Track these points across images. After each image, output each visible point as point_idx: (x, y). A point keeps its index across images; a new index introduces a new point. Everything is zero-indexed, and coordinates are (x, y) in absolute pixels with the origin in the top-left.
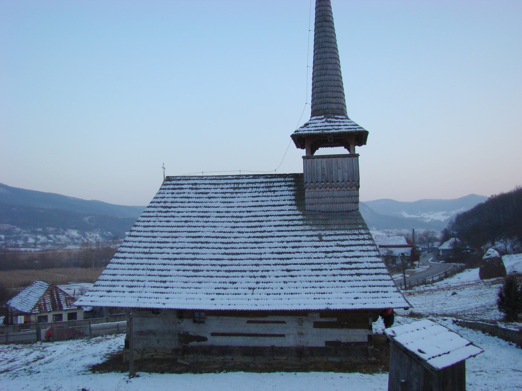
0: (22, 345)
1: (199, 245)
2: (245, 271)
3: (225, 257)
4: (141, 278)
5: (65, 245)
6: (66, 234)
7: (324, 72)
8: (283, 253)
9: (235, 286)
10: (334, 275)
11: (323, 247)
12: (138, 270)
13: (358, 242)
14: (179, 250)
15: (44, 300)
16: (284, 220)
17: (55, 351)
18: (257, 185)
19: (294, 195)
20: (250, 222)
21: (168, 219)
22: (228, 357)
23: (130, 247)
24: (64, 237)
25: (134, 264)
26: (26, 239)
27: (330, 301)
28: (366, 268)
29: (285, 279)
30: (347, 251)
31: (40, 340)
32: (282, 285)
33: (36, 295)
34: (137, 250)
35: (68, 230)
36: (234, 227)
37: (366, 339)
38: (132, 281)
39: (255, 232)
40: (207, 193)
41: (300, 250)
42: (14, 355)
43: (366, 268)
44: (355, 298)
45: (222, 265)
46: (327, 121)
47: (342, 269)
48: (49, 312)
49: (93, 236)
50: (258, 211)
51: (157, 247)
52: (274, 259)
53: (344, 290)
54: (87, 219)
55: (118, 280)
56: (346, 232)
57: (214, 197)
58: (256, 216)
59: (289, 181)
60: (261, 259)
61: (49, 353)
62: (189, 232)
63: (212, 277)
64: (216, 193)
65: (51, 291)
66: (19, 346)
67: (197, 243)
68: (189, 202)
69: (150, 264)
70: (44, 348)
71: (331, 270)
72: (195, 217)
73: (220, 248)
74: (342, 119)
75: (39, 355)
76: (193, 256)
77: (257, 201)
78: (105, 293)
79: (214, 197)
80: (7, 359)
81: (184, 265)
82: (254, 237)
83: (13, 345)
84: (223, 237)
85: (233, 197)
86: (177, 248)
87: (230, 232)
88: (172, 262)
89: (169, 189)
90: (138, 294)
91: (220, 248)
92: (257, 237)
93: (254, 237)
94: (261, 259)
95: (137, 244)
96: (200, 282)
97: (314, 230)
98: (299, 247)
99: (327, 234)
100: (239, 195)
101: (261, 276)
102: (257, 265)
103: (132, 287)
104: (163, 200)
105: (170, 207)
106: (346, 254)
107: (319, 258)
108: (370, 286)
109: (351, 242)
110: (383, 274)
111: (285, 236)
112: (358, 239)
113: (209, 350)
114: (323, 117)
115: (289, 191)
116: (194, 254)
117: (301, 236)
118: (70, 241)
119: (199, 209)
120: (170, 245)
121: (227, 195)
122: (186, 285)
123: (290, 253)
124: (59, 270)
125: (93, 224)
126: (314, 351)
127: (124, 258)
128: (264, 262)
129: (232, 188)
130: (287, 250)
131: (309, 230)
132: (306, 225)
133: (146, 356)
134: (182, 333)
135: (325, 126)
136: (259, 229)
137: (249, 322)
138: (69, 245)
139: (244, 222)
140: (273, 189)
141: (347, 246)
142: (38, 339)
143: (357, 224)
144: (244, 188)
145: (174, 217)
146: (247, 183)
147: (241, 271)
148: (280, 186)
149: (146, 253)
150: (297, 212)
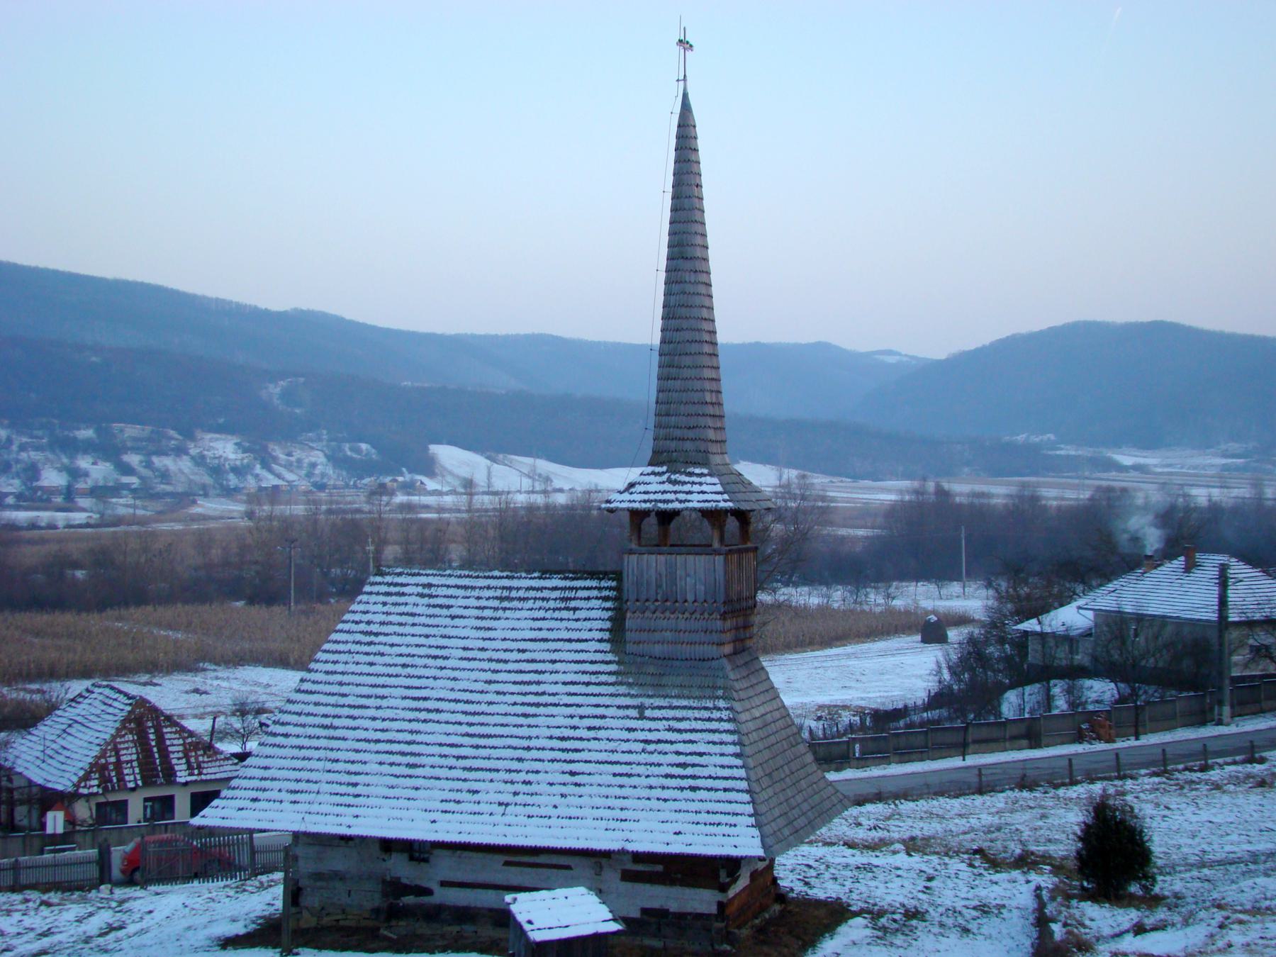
1: (423, 715)
2: (498, 770)
3: (466, 740)
4: (314, 776)
5: (187, 498)
6: (193, 452)
7: (673, 371)
8: (569, 738)
9: (476, 797)
10: (651, 787)
12: (310, 759)
14: (386, 724)
15: (117, 751)
16: (584, 672)
17: (150, 912)
18: (546, 594)
19: (610, 619)
20: (521, 672)
21: (371, 658)
22: (468, 928)
23: (297, 714)
24: (185, 464)
26: (33, 472)
27: (632, 836)
28: (710, 777)
29: (564, 790)
30: (684, 742)
31: (110, 881)
33: (89, 735)
34: (310, 720)
35: (199, 434)
36: (489, 682)
37: (713, 909)
39: (525, 694)
40: (449, 607)
41: (601, 734)
42: (48, 921)
43: (710, 777)
45: (458, 758)
46: (670, 481)
47: (667, 776)
48: (133, 789)
49: (299, 461)
51: (348, 717)
52: (552, 749)
53: (662, 816)
55: (273, 779)
57: (462, 617)
58: (533, 661)
59: (606, 588)
60: (529, 749)
61: (136, 916)
62: (408, 687)
63: (439, 779)
65: (139, 721)
66: (54, 897)
68: (414, 625)
69: (332, 749)
70: (121, 902)
71: (647, 776)
73: (460, 723)
74: (702, 475)
75: (111, 921)
76: (409, 737)
77: (540, 629)
78: (248, 804)
79: (462, 617)
80: (32, 929)
82: (523, 704)
83: (34, 895)
84: (467, 702)
85: (495, 619)
86: (384, 720)
87: (482, 692)
88: (373, 747)
89: (378, 594)
90: (306, 807)
91: (460, 723)
92: (529, 704)
93: (523, 704)
94: (529, 749)
95: (311, 709)
96: (417, 789)
98: (600, 728)
101: (524, 782)
102: (520, 760)
103: (296, 792)
104: (366, 618)
105: (377, 634)
106: (681, 747)
107: (630, 752)
108: (708, 812)
109: (695, 725)
110: (738, 791)
111: (578, 706)
112: (709, 720)
113: (435, 914)
114: (664, 469)
115: (604, 609)
116: (411, 732)
118: (208, 480)
119: (432, 641)
120: (371, 712)
121: (487, 613)
123: (581, 739)
124: (166, 613)
125: (297, 411)
127: (286, 735)
128: (534, 754)
129: (497, 598)
130: (577, 733)
131: (625, 695)
132: (621, 684)
133: (326, 921)
134: (388, 878)
135: (664, 492)
136: (534, 688)
137: (507, 864)
138: (206, 495)
139: (509, 672)
140: (573, 604)
141: (686, 731)
142: (104, 876)
143: (715, 688)
144: (520, 599)
145: (382, 654)
146: (528, 589)
147: (490, 770)
148: (588, 599)
149: (326, 727)
150: (610, 657)
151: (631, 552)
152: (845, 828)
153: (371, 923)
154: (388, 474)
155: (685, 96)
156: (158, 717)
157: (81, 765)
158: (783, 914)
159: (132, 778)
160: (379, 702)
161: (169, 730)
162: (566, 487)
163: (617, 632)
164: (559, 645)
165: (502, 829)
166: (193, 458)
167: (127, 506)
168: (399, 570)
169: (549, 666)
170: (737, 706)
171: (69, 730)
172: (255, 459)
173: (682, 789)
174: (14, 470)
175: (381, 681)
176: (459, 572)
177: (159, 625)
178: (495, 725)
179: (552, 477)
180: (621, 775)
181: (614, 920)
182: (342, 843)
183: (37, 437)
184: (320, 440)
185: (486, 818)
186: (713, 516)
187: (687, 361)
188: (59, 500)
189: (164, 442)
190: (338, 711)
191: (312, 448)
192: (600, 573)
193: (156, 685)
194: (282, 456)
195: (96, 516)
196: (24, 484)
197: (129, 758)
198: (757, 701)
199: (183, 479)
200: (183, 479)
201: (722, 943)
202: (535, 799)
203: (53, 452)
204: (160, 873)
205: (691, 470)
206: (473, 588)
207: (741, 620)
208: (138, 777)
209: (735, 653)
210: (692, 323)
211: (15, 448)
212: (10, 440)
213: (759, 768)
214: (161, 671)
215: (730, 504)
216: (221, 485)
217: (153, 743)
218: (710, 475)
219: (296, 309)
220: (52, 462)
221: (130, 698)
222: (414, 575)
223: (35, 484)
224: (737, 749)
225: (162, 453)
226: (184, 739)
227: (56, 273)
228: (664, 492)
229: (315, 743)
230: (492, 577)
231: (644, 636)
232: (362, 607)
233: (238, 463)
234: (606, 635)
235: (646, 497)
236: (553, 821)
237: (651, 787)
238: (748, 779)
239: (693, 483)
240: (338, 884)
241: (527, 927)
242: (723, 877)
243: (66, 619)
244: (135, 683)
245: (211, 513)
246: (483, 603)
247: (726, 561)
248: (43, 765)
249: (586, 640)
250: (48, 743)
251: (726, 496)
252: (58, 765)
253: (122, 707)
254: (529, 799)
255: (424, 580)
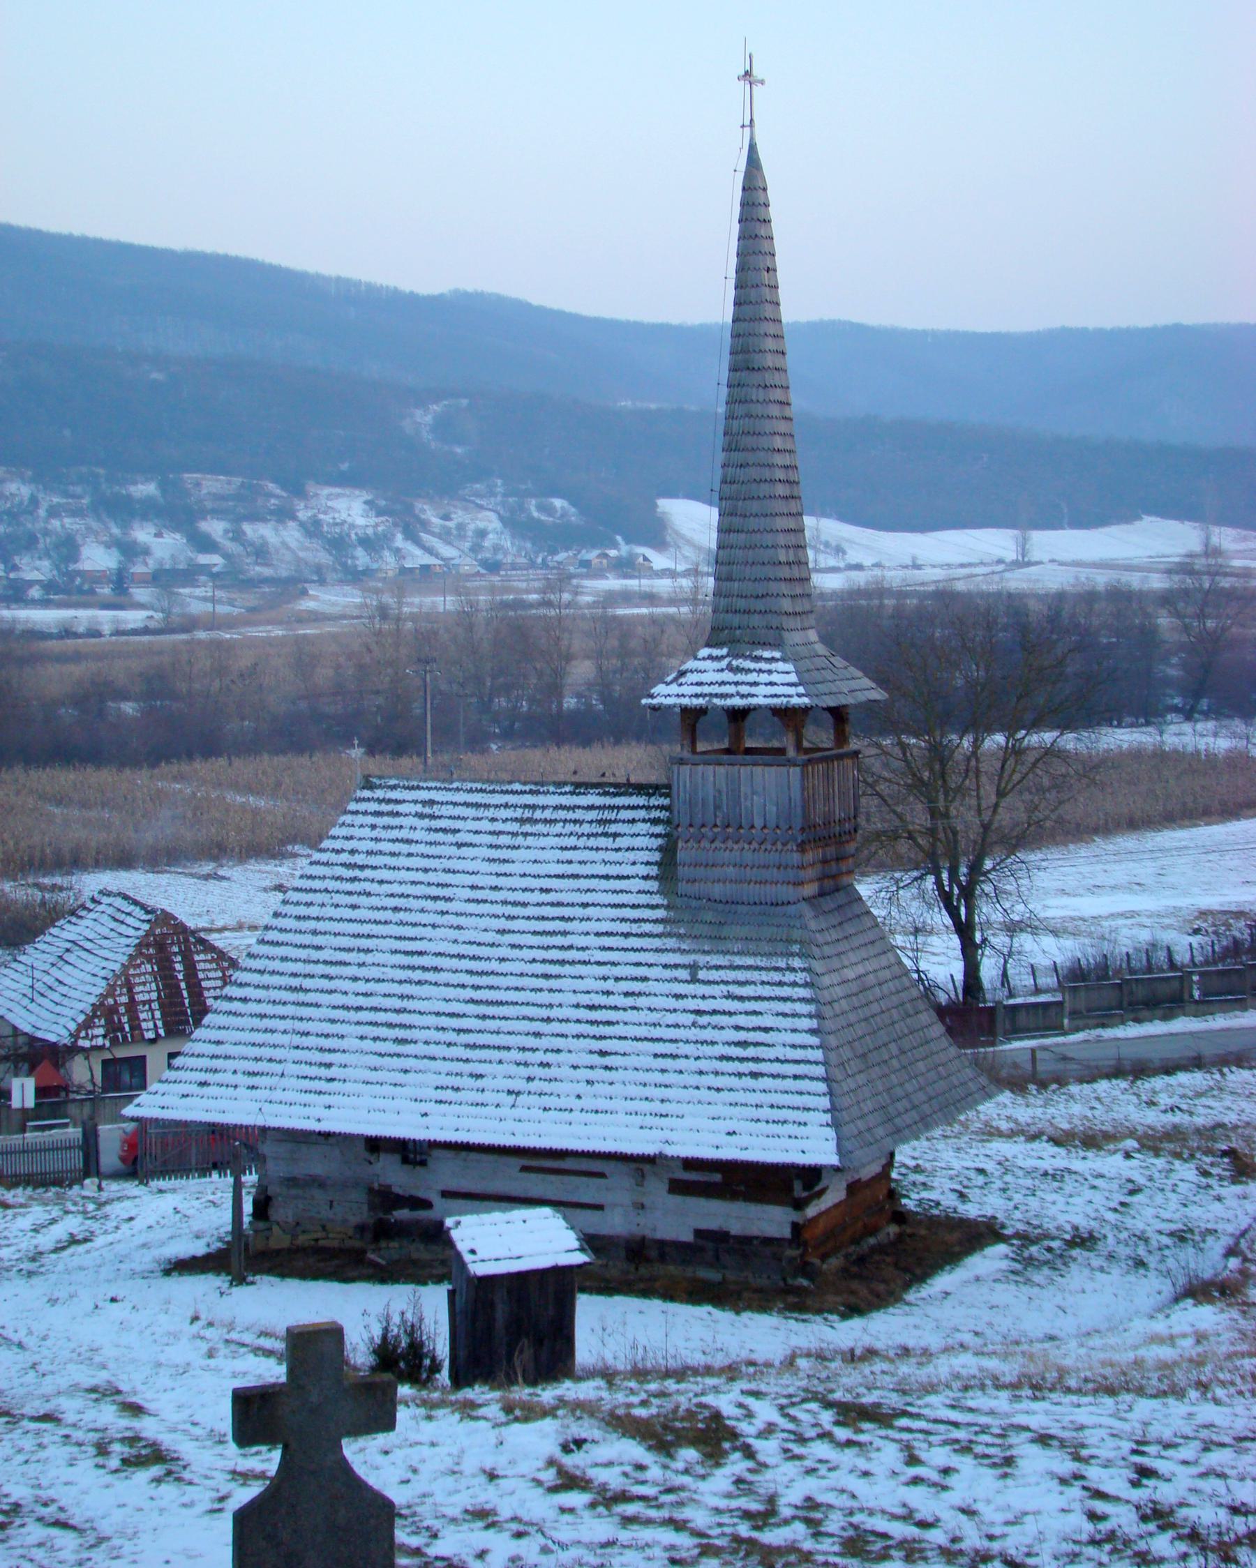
0: (29, 1190)
1: (418, 975)
2: (509, 1048)
4: (278, 1053)
5: (293, 586)
8: (600, 1007)
9: (480, 1083)
10: (701, 1073)
11: (694, 997)
12: (272, 1031)
13: (779, 991)
14: (371, 987)
16: (623, 920)
17: (131, 1219)
18: (579, 814)
19: (660, 849)
20: (543, 918)
24: (291, 534)
25: (265, 1016)
26: (68, 548)
29: (591, 1074)
30: (747, 1013)
31: (98, 1174)
32: (582, 1088)
34: (276, 980)
35: (311, 488)
36: (502, 932)
37: (786, 1232)
38: (257, 1059)
41: (642, 1002)
43: (777, 1060)
44: (729, 1134)
45: (459, 1031)
46: (730, 668)
47: (722, 1058)
48: (153, 1041)
49: (461, 527)
50: (567, 891)
52: (578, 1021)
53: (713, 1110)
54: (424, 418)
55: (227, 1057)
56: (758, 961)
58: (559, 904)
59: (656, 807)
60: (548, 1020)
62: (400, 938)
63: (434, 1058)
64: (476, 832)
65: (161, 946)
67: (413, 968)
68: (410, 855)
71: (698, 1058)
72: (417, 897)
73: (463, 986)
74: (773, 660)
75: (75, 1231)
76: (398, 1003)
77: (570, 862)
78: (194, 1089)
81: (376, 1024)
82: (544, 961)
84: (474, 958)
86: (368, 981)
87: (493, 945)
89: (365, 813)
91: (463, 986)
92: (552, 962)
93: (544, 961)
94: (548, 1020)
96: (406, 1071)
97: (683, 952)
98: (640, 994)
99: (713, 963)
100: (530, 841)
101: (541, 1064)
102: (537, 1035)
103: (254, 1074)
105: (362, 867)
106: (742, 1020)
107: (677, 1026)
108: (772, 1106)
110: (812, 1079)
111: (614, 964)
112: (781, 984)
114: (724, 651)
115: (652, 835)
116: (402, 997)
117: (650, 965)
118: (324, 558)
119: (432, 877)
121: (504, 840)
122: (373, 1076)
123: (615, 1008)
124: (245, 768)
125: (459, 450)
126: (666, 1250)
127: (245, 1000)
128: (556, 1027)
131: (673, 951)
132: (669, 935)
133: (302, 1239)
134: (376, 1186)
135: (723, 683)
136: (559, 940)
137: (525, 1169)
138: (322, 582)
139: (528, 918)
140: (613, 828)
141: (749, 998)
142: (91, 1167)
143: (789, 941)
144: (546, 821)
145: (369, 894)
146: (556, 808)
148: (633, 821)
150: (657, 899)
151: (682, 762)
152: (1131, 1108)
153: (357, 1244)
154: (594, 547)
155: (752, 148)
156: (186, 940)
157: (81, 1006)
158: (900, 1237)
159: (151, 1025)
160: (362, 957)
161: (202, 957)
162: (867, 562)
163: (667, 866)
164: (593, 883)
165: (510, 1125)
166: (302, 525)
167: (205, 599)
168: (392, 782)
169: (579, 912)
170: (818, 966)
171: (67, 956)
172: (395, 525)
173: (740, 1075)
174: (41, 546)
175: (365, 929)
176: (469, 785)
177: (235, 786)
178: (508, 989)
179: (845, 546)
180: (664, 1056)
181: (582, 1249)
182: (322, 1139)
183: (73, 496)
184: (492, 494)
185: (490, 1110)
186: (788, 716)
187: (755, 507)
188: (106, 591)
189: (260, 502)
190: (310, 968)
191: (481, 507)
192: (650, 786)
193: (223, 878)
194: (436, 521)
195: (159, 616)
196: (57, 567)
197: (147, 997)
198: (853, 957)
199: (288, 556)
200: (288, 556)
201: (795, 1277)
202: (554, 1087)
203: (99, 519)
204: (165, 1163)
205: (759, 653)
206: (487, 806)
207: (831, 851)
208: (160, 1024)
209: (822, 894)
210: (761, 456)
211: (42, 512)
212: (34, 501)
213: (847, 1047)
214: (231, 858)
215: (806, 700)
216: (344, 565)
217: (181, 977)
218: (783, 660)
219: (456, 291)
220: (96, 534)
221: (148, 912)
222: (413, 788)
223: (72, 567)
224: (814, 1023)
225: (254, 518)
226: (223, 970)
227: (100, 244)
228: (723, 683)
229: (280, 1010)
230: (513, 792)
231: (700, 872)
232: (344, 831)
233: (370, 531)
234: (654, 871)
235: (698, 690)
236: (575, 1115)
237: (701, 1073)
238: (825, 1063)
239: (760, 671)
240: (318, 1194)
241: (468, 1257)
242: (798, 1191)
243: (102, 777)
244: (192, 875)
245: (328, 610)
246: (499, 826)
247: (804, 776)
248: (32, 1006)
249: (628, 877)
250: (37, 974)
251: (801, 690)
252: (51, 1006)
253: (137, 926)
254: (546, 1087)
255: (424, 795)
